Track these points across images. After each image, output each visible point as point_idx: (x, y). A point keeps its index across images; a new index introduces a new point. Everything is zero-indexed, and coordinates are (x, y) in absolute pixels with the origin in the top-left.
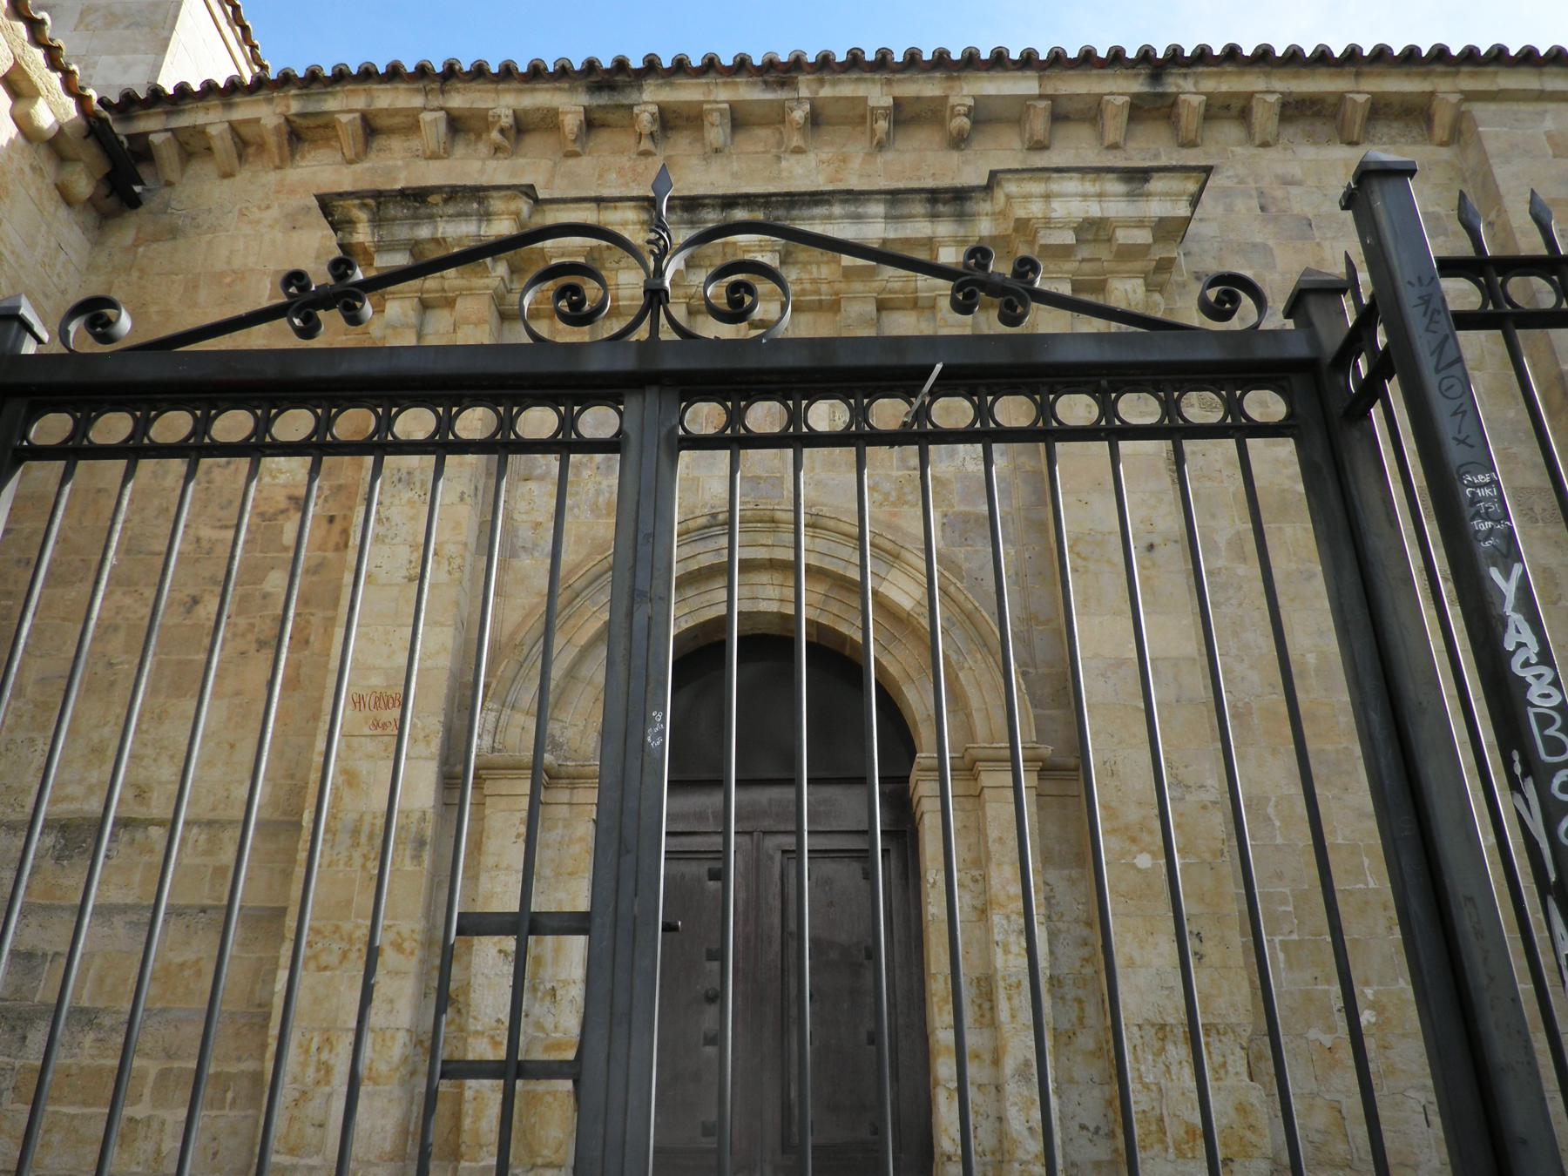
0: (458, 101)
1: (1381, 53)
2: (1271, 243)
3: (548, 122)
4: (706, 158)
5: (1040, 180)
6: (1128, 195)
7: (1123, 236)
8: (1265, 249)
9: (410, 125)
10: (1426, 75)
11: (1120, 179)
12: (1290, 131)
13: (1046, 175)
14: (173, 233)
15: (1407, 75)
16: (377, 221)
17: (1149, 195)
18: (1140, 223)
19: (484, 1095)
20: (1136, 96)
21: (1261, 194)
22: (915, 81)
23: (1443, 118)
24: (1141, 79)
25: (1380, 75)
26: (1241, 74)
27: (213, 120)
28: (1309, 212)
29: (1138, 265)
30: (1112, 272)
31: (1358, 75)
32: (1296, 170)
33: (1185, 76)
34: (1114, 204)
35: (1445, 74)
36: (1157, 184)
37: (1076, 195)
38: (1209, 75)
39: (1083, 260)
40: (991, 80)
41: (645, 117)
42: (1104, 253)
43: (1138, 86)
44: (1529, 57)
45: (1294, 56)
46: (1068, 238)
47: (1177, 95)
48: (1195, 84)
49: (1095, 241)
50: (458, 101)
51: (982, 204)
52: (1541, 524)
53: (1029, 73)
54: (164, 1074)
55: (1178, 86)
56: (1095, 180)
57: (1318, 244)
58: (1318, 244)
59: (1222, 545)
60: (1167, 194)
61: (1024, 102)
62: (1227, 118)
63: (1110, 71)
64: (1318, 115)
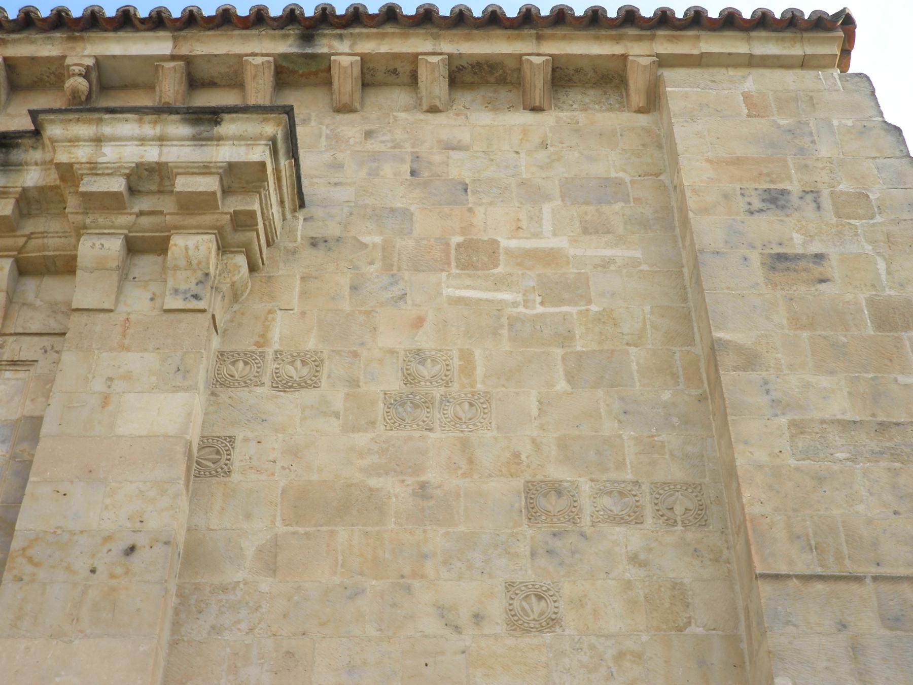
2: (413, 208)
5: (89, 121)
6: (194, 138)
7: (183, 184)
8: (406, 215)
10: (618, 39)
11: (185, 121)
12: (465, 98)
13: (96, 115)
15: (597, 38)
17: (220, 139)
18: (205, 169)
20: (285, 56)
21: (416, 158)
22: (33, 42)
23: (637, 82)
24: (290, 41)
25: (564, 38)
26: (406, 36)
29: (208, 219)
30: (176, 227)
31: (539, 38)
32: (464, 136)
33: (341, 37)
34: (174, 146)
35: (639, 38)
36: (230, 127)
37: (132, 138)
38: (368, 37)
39: (141, 213)
40: (119, 40)
42: (167, 204)
43: (284, 45)
46: (118, 185)
47: (327, 56)
48: (351, 47)
49: (160, 192)
51: (31, 152)
52: (679, 527)
53: (161, 34)
55: (330, 47)
56: (155, 122)
57: (470, 210)
58: (470, 210)
59: (250, 552)
60: (241, 138)
61: (153, 62)
62: (398, 85)
63: (254, 32)
64: (502, 81)
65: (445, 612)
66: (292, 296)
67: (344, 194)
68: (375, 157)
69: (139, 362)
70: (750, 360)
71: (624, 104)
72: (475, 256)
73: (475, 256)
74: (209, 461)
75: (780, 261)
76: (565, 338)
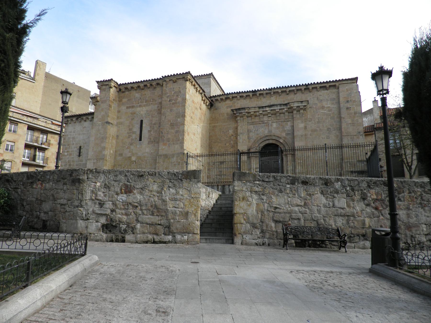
1: (330, 81)
3: (249, 95)
7: (301, 107)
8: (317, 104)
9: (236, 97)
14: (216, 109)
16: (236, 111)
19: (244, 158)
27: (219, 98)
28: (322, 99)
32: (321, 94)
41: (258, 95)
43: (305, 87)
44: (346, 80)
45: (321, 83)
50: (240, 95)
54: (102, 123)
65: (322, 138)
66: (309, 113)
67: (312, 102)
68: (314, 97)
69: (299, 121)
70: (344, 118)
71: (336, 89)
72: (323, 108)
73: (323, 108)
74: (305, 128)
75: (347, 108)
76: (330, 115)
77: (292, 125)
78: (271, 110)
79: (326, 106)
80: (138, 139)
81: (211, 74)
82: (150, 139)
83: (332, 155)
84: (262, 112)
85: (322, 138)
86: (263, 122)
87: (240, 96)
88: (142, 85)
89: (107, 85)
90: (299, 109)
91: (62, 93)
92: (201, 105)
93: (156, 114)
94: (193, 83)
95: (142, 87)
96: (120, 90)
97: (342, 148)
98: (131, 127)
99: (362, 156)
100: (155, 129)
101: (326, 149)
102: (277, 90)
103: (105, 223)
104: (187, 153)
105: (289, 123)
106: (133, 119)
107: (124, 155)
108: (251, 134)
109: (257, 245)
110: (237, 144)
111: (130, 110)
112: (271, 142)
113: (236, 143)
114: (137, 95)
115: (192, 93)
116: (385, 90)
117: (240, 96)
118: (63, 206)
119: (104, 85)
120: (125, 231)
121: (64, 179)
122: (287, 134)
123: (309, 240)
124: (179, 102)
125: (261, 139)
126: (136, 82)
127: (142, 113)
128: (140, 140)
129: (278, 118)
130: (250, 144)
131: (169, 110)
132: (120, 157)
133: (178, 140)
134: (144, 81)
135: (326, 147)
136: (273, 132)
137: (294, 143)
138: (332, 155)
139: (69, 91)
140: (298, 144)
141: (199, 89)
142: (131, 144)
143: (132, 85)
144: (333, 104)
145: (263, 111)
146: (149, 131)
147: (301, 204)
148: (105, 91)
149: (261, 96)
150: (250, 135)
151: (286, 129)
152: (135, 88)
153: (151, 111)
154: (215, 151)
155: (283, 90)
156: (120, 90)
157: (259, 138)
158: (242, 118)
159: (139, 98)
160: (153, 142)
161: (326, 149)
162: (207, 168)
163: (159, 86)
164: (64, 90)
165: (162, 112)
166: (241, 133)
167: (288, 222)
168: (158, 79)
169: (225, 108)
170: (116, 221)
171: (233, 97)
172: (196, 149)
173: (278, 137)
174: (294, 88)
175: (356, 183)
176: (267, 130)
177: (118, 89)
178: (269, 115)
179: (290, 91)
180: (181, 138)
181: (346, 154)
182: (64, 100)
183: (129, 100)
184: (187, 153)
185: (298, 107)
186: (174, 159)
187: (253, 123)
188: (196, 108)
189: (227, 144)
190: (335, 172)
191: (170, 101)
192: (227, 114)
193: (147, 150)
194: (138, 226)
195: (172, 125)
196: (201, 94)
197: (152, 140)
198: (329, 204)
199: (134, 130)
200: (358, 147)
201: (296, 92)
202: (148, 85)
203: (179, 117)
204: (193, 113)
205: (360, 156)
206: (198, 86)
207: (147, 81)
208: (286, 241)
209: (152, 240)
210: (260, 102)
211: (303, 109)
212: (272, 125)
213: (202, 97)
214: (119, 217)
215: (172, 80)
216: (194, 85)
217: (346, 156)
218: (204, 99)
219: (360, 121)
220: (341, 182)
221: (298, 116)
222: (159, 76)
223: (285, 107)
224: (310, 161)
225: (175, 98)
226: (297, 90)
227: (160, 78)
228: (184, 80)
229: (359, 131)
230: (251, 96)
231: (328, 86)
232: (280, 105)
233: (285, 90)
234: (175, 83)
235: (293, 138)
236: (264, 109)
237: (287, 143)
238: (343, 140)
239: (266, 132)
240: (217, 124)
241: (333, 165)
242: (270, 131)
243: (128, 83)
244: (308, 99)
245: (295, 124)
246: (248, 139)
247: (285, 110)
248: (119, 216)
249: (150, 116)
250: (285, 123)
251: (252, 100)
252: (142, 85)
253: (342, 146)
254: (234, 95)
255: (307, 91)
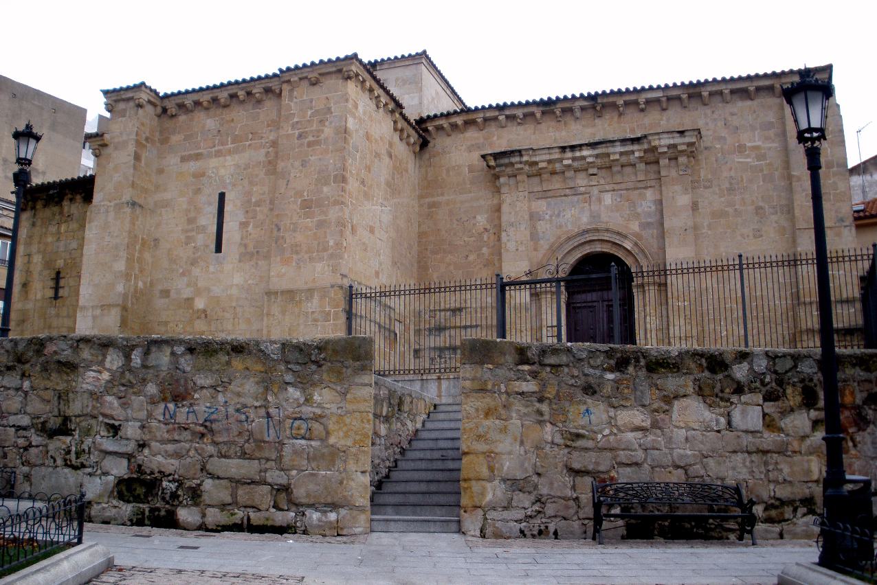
0: (508, 112)
3: (533, 114)
4: (575, 121)
7: (680, 148)
8: (724, 138)
9: (496, 119)
16: (495, 159)
18: (684, 144)
21: (725, 119)
32: (735, 110)
45: (732, 79)
50: (508, 112)
67: (710, 133)
69: (678, 188)
72: (741, 149)
73: (741, 149)
76: (762, 170)
77: (658, 197)
78: (597, 156)
79: (749, 144)
80: (213, 246)
81: (424, 54)
82: (246, 246)
83: (770, 285)
84: (569, 162)
85: (742, 235)
86: (575, 191)
87: (508, 117)
88: (223, 95)
89: (131, 99)
90: (674, 154)
91: (17, 135)
92: (391, 145)
93: (262, 174)
94: (368, 84)
95: (222, 101)
96: (165, 110)
97: (796, 265)
98: (192, 215)
99: (850, 287)
100: (260, 217)
101: (741, 269)
102: (611, 99)
103: (126, 477)
104: (351, 287)
105: (649, 194)
106: (198, 191)
107: (173, 294)
108: (542, 226)
109: (525, 536)
110: (500, 254)
111: (193, 166)
112: (598, 248)
113: (498, 252)
114: (208, 122)
115: (365, 113)
116: (816, 130)
117: (508, 117)
118: (21, 433)
119: (123, 100)
120: (174, 496)
121: (24, 363)
122: (644, 226)
123: (664, 518)
124: (327, 138)
125: (569, 239)
126: (208, 88)
127: (222, 172)
128: (218, 249)
129: (618, 178)
130: (539, 256)
131: (297, 164)
132: (163, 301)
133: (325, 250)
134: (230, 84)
135: (741, 264)
136: (604, 218)
137: (663, 249)
138: (770, 285)
139: (34, 131)
140: (677, 254)
141: (384, 99)
142: (194, 262)
143: (195, 97)
144: (767, 138)
145: (574, 159)
146: (244, 225)
147: (644, 424)
148: (124, 116)
149: (568, 117)
150: (540, 231)
151: (639, 210)
152: (205, 104)
153: (247, 167)
154: (435, 277)
155: (628, 98)
156: (165, 110)
157: (564, 237)
158: (512, 181)
159: (215, 132)
160: (252, 255)
161: (741, 269)
162: (412, 327)
163: (270, 95)
164: (21, 128)
165: (279, 169)
166: (512, 225)
167: (607, 472)
168: (267, 77)
169: (461, 154)
170: (152, 473)
171: (486, 120)
172: (377, 274)
173: (618, 233)
174: (659, 94)
175: (789, 363)
176: (587, 214)
177: (159, 110)
178: (591, 171)
179: (648, 102)
180: (331, 243)
181: (806, 281)
182: (22, 155)
183: (187, 138)
184: (351, 287)
185: (669, 147)
186: (314, 305)
187: (545, 195)
188: (378, 155)
189: (471, 258)
190: (780, 331)
191: (300, 136)
192: (471, 169)
193: (238, 279)
194: (208, 484)
195: (307, 205)
196: (392, 112)
197: (251, 248)
198: (717, 421)
199: (203, 221)
200: (838, 262)
201: (664, 105)
202: (241, 94)
203: (327, 184)
204: (368, 169)
205: (843, 285)
206: (381, 92)
207: (237, 83)
208: (598, 520)
209: (245, 521)
210: (564, 133)
211: (687, 152)
212: (599, 200)
213: (395, 122)
214: (159, 462)
215: (306, 78)
216: (371, 90)
217: (806, 286)
218: (399, 126)
219: (842, 186)
220: (751, 363)
221: (673, 173)
222: (272, 69)
223: (636, 147)
224: (710, 302)
225: (314, 127)
226: (669, 99)
227: (275, 75)
228: (340, 76)
229: (840, 216)
230: (538, 115)
231: (752, 89)
232: (624, 141)
233: (633, 97)
234: (316, 88)
235: (662, 236)
236: (578, 154)
237: (643, 251)
238: (799, 241)
239: (585, 221)
240: (439, 199)
241: (772, 314)
242: (595, 216)
243: (187, 92)
244: (701, 124)
245: (664, 193)
246: (532, 240)
247: (637, 154)
248: (157, 460)
249: (246, 182)
250: (637, 192)
251: (543, 126)
252: (223, 95)
253: (795, 261)
254: (489, 114)
255: (694, 103)
